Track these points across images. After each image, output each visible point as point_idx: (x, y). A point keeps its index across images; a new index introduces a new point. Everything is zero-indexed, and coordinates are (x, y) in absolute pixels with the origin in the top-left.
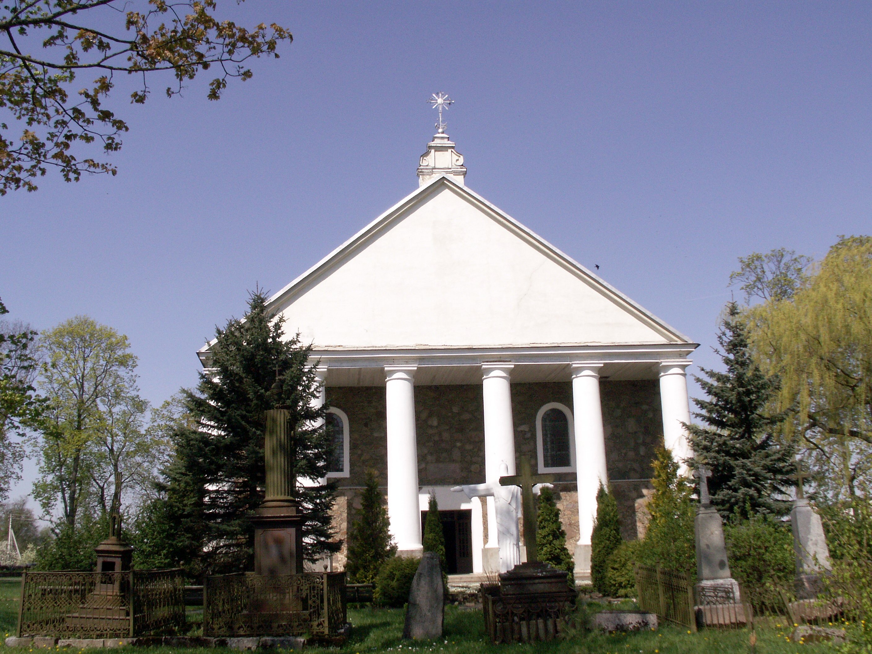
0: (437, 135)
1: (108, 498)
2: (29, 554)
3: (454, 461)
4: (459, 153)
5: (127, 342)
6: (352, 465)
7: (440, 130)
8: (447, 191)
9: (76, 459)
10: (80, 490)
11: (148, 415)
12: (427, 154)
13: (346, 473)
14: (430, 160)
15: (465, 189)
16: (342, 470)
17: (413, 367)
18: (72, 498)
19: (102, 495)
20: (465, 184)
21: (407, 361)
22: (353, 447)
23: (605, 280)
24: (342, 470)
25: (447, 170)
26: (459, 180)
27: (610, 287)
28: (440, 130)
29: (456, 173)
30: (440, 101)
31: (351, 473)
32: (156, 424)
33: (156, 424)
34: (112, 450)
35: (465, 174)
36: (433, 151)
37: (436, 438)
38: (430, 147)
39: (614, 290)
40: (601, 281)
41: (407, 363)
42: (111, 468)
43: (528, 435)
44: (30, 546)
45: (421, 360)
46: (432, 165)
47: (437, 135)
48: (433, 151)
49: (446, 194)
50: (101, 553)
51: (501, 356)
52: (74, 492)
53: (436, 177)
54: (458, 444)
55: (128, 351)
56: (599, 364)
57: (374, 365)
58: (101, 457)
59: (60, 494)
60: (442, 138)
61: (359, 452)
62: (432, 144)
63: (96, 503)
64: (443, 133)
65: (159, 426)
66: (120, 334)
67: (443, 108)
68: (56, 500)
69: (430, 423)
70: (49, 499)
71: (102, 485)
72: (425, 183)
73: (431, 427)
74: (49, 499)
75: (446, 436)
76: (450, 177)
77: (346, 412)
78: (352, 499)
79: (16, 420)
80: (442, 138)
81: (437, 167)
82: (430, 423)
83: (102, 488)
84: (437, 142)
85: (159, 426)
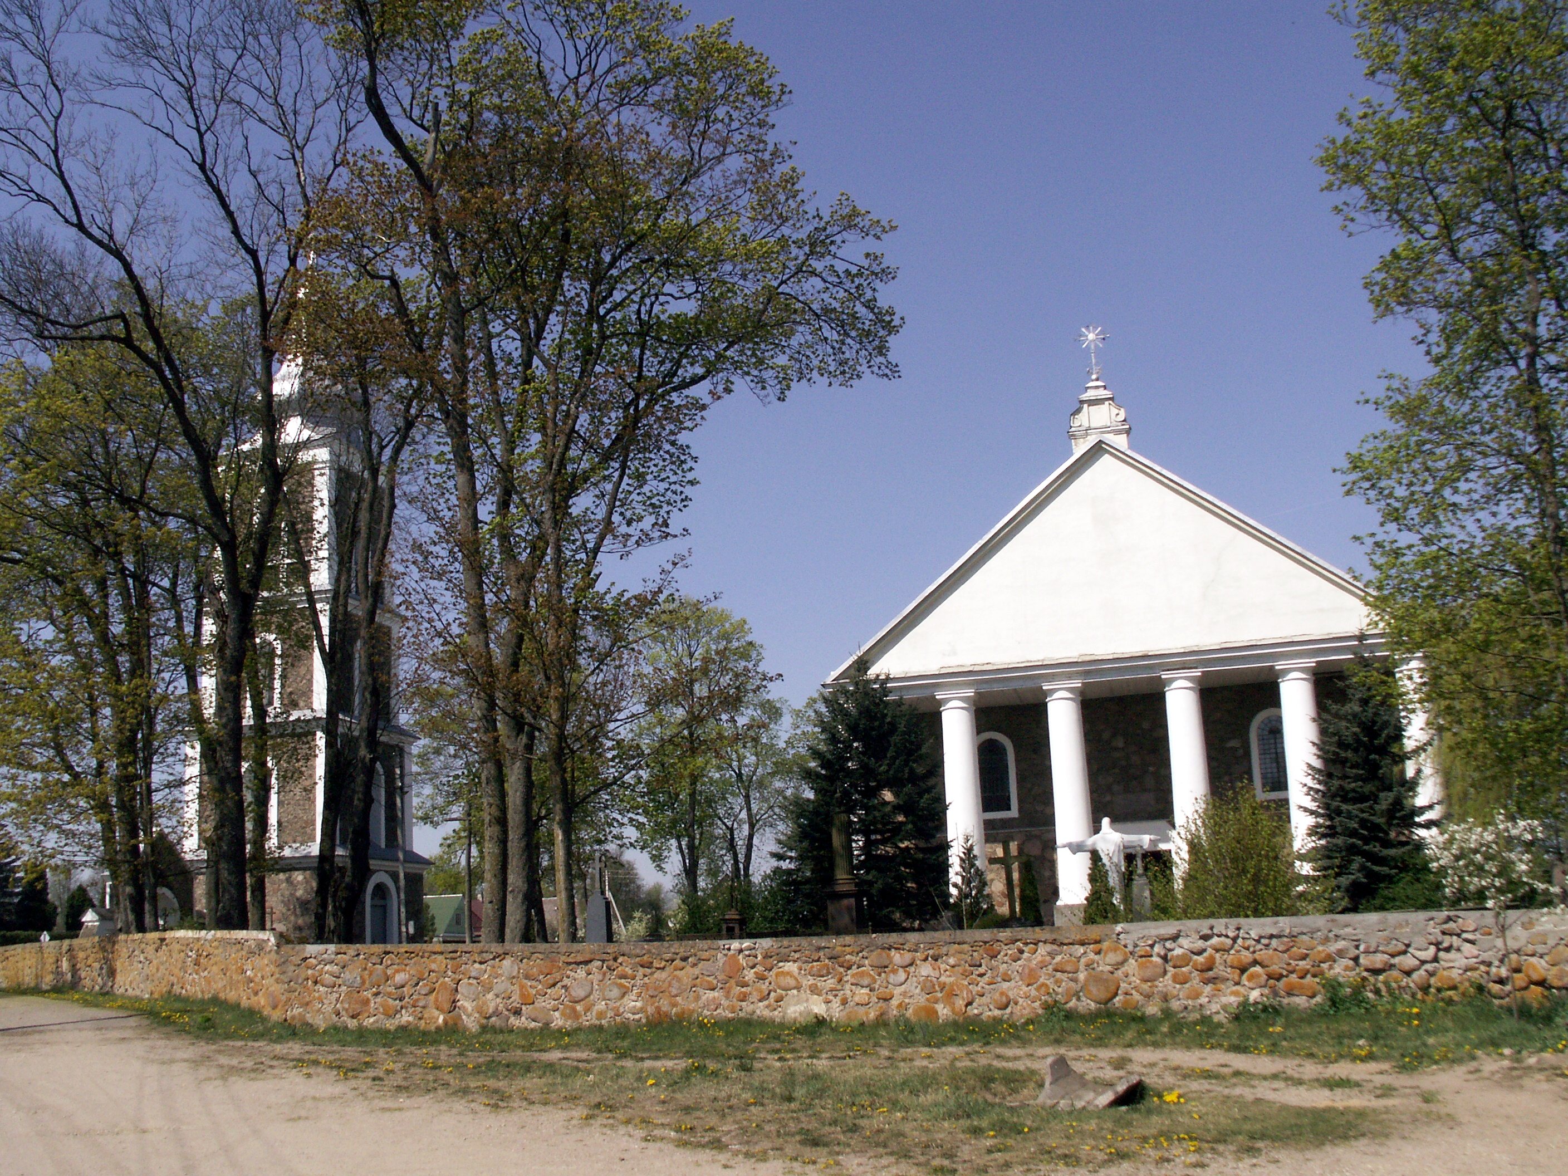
0: (1091, 384)
1: (740, 843)
2: (636, 926)
3: (1145, 790)
4: (1119, 406)
5: (746, 627)
6: (1021, 801)
7: (1094, 377)
8: (1107, 457)
9: (692, 795)
10: (701, 834)
11: (787, 721)
12: (1078, 411)
13: (1014, 813)
14: (1082, 420)
15: (1129, 452)
16: (1009, 809)
17: (1077, 684)
18: (691, 847)
19: (732, 839)
20: (1130, 447)
21: (1070, 676)
22: (1021, 780)
23: (1315, 553)
24: (1009, 809)
25: (1105, 429)
26: (1121, 442)
27: (1321, 562)
28: (1094, 377)
29: (1118, 432)
30: (1091, 336)
31: (1020, 811)
32: (799, 732)
33: (799, 732)
34: (739, 775)
35: (1128, 432)
36: (1085, 406)
37: (1124, 763)
38: (1082, 402)
39: (1326, 566)
40: (1309, 555)
41: (1070, 678)
42: (741, 800)
43: (1241, 752)
44: (637, 914)
45: (1087, 673)
46: (1086, 425)
47: (1091, 384)
48: (1085, 406)
49: (1106, 461)
50: (726, 921)
51: (1184, 662)
52: (692, 839)
53: (1091, 441)
54: (1151, 769)
55: (749, 638)
56: (1311, 662)
57: (1029, 684)
58: (724, 789)
59: (673, 842)
60: (1097, 387)
61: (1029, 786)
62: (1084, 397)
63: (724, 852)
64: (1097, 379)
65: (804, 733)
66: (736, 617)
67: (1096, 346)
68: (670, 850)
69: (1114, 744)
70: (659, 849)
71: (729, 824)
72: (1080, 448)
73: (1116, 749)
74: (659, 849)
75: (1135, 759)
76: (1110, 438)
77: (1010, 737)
78: (1023, 843)
79: (392, 311)
80: (1097, 387)
81: (1093, 426)
82: (1114, 744)
83: (731, 830)
84: (1090, 394)
85: (804, 733)
